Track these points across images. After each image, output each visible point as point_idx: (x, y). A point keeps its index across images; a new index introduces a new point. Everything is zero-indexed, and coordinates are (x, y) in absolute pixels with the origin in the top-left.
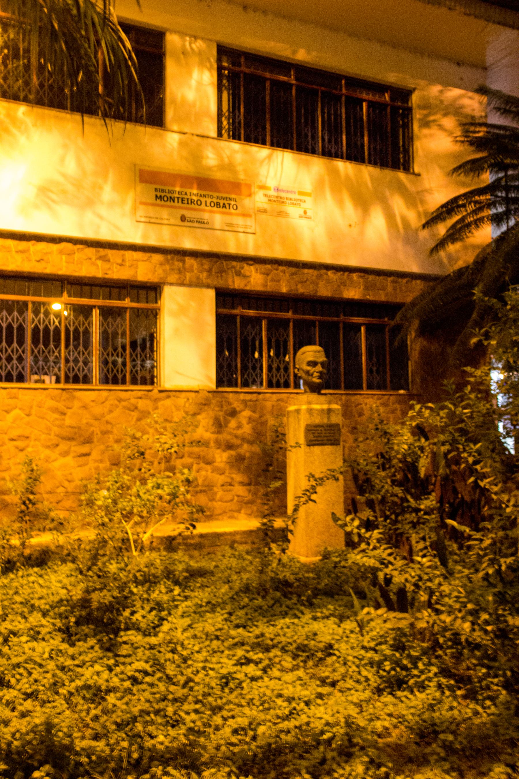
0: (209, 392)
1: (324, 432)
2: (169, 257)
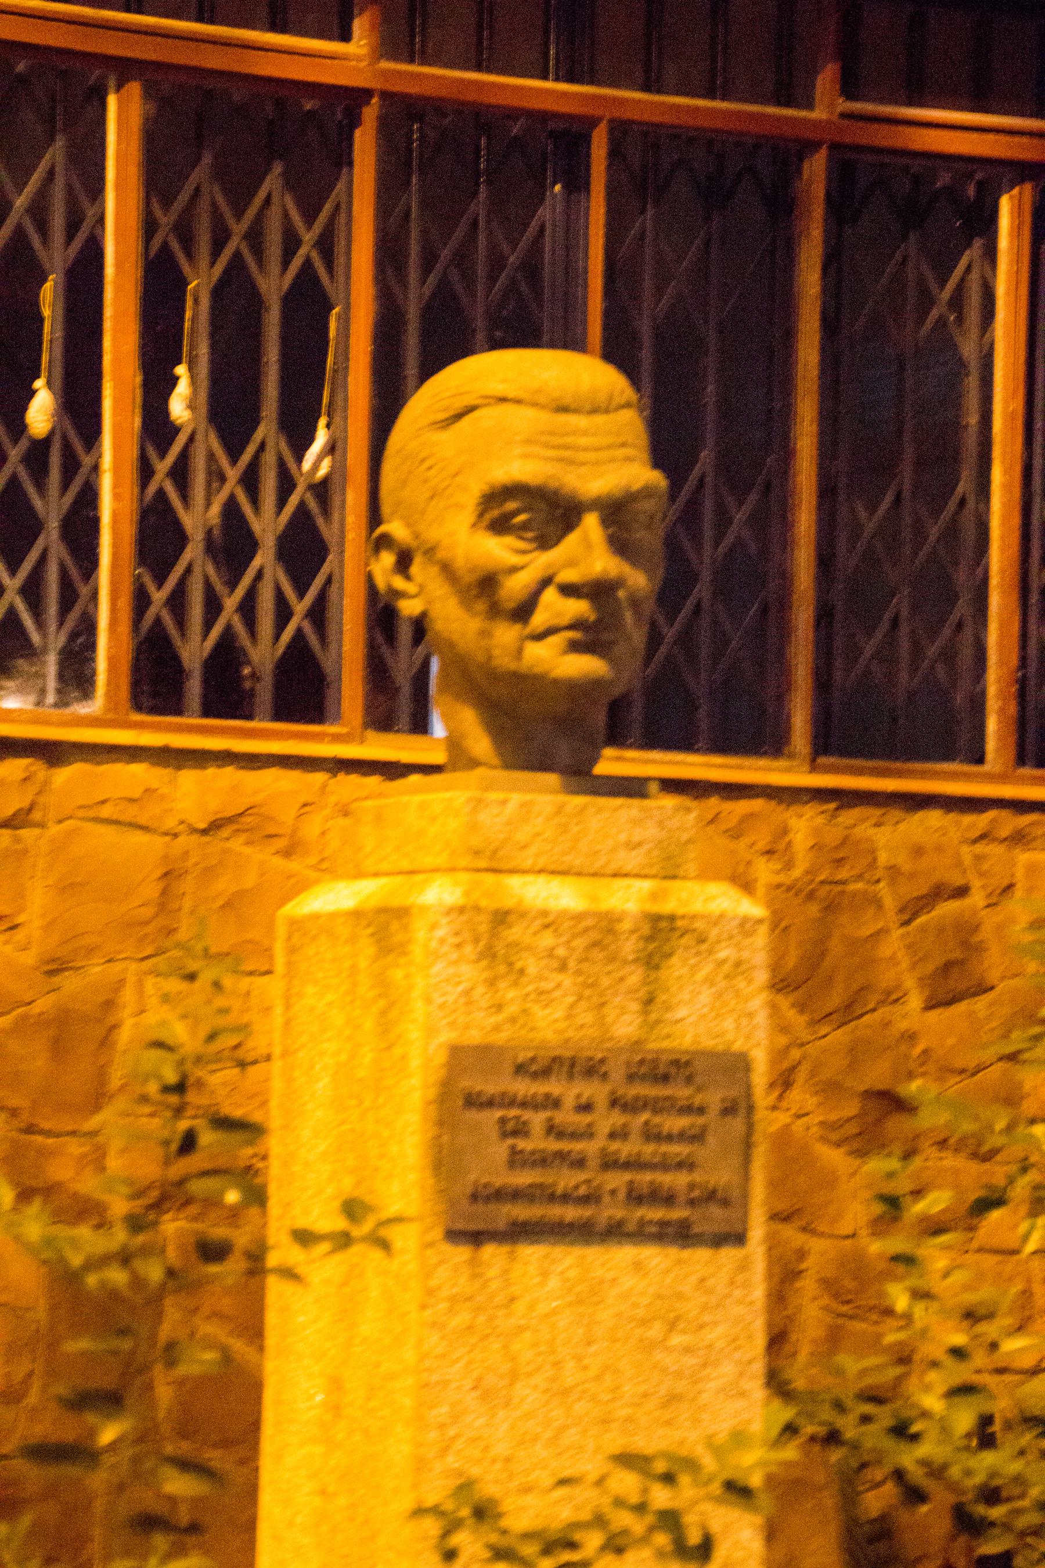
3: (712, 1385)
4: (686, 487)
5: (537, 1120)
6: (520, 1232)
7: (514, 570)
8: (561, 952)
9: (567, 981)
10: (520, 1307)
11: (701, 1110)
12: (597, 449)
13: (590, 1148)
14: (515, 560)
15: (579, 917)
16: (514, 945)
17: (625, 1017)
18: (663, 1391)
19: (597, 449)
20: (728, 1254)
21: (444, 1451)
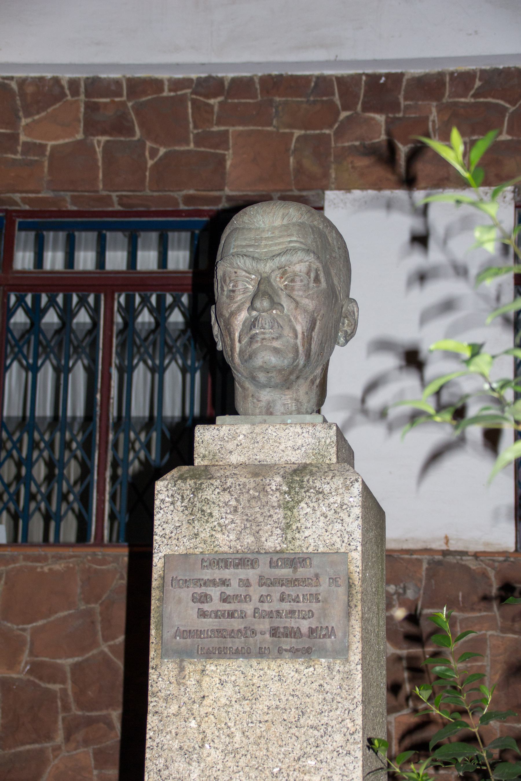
4: (358, 635)
5: (215, 592)
13: (249, 608)
16: (207, 501)
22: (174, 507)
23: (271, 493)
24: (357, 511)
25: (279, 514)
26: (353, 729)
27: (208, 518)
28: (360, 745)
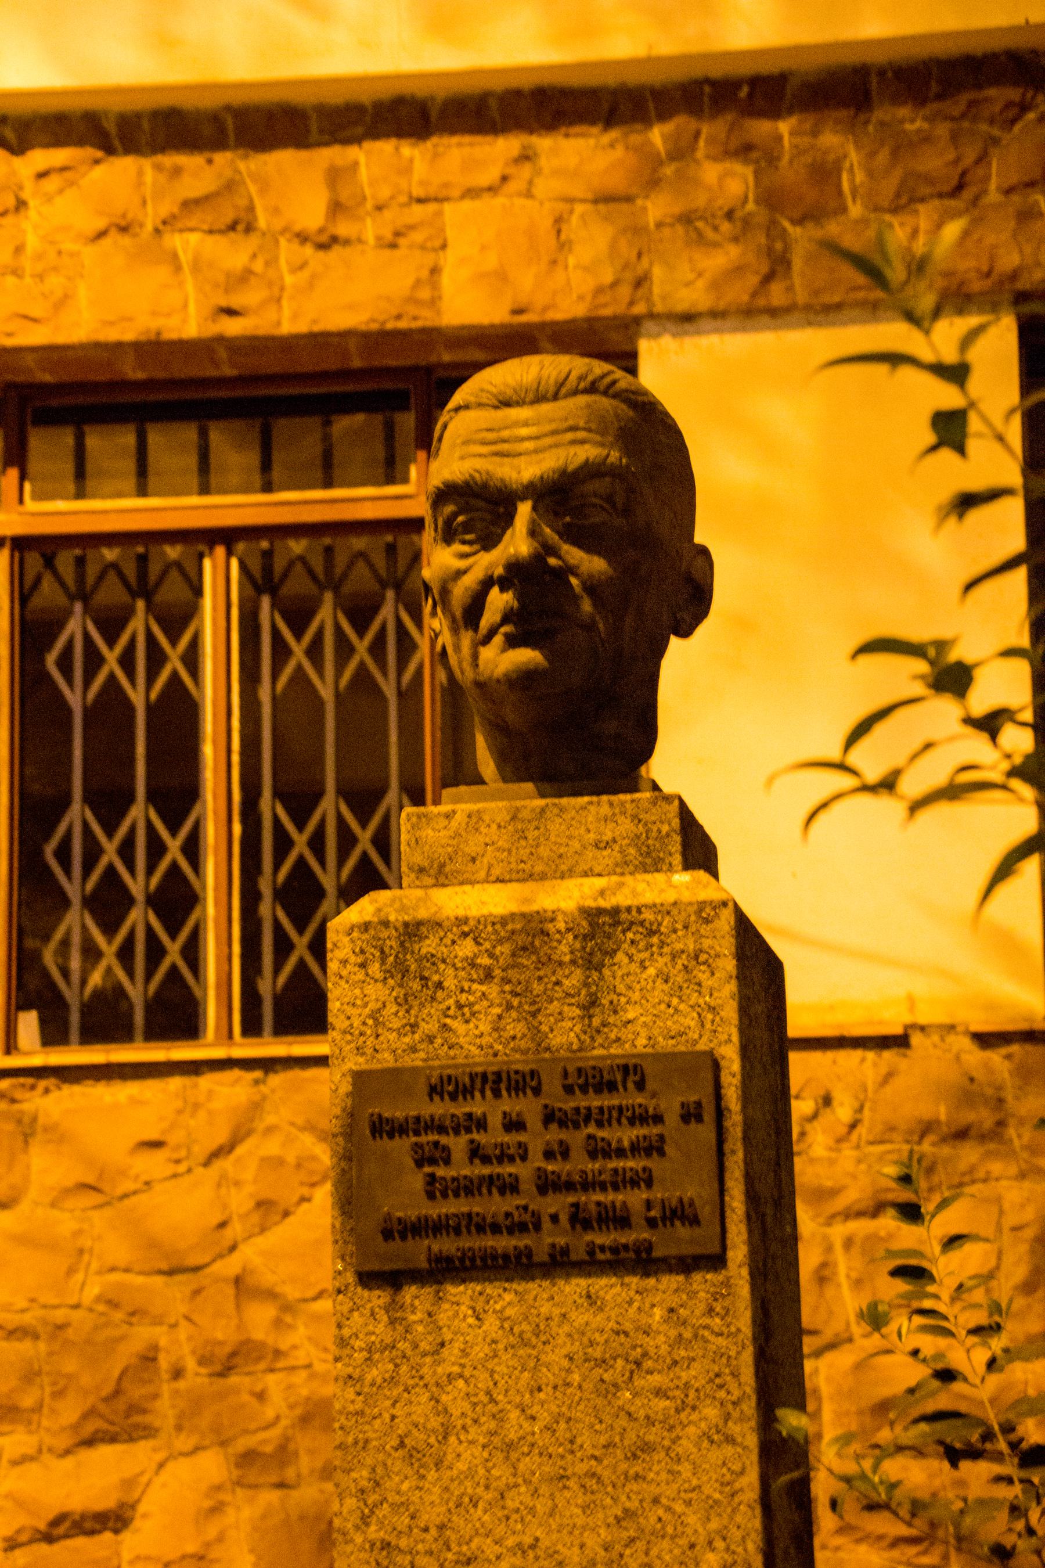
0: (984, 1040)
1: (538, 1138)
2: (657, 135)
3: (692, 1430)
5: (458, 1144)
6: (443, 1271)
7: (460, 573)
8: (484, 961)
9: (492, 990)
10: (452, 1353)
11: (658, 1119)
12: (537, 438)
13: (523, 1171)
14: (462, 564)
15: (504, 921)
17: (564, 1024)
18: (631, 1437)
19: (537, 438)
20: (703, 1281)
21: (365, 1520)
22: (367, 975)
23: (558, 936)
24: (729, 965)
25: (572, 980)
26: (736, 1393)
27: (435, 992)
28: (753, 1423)
